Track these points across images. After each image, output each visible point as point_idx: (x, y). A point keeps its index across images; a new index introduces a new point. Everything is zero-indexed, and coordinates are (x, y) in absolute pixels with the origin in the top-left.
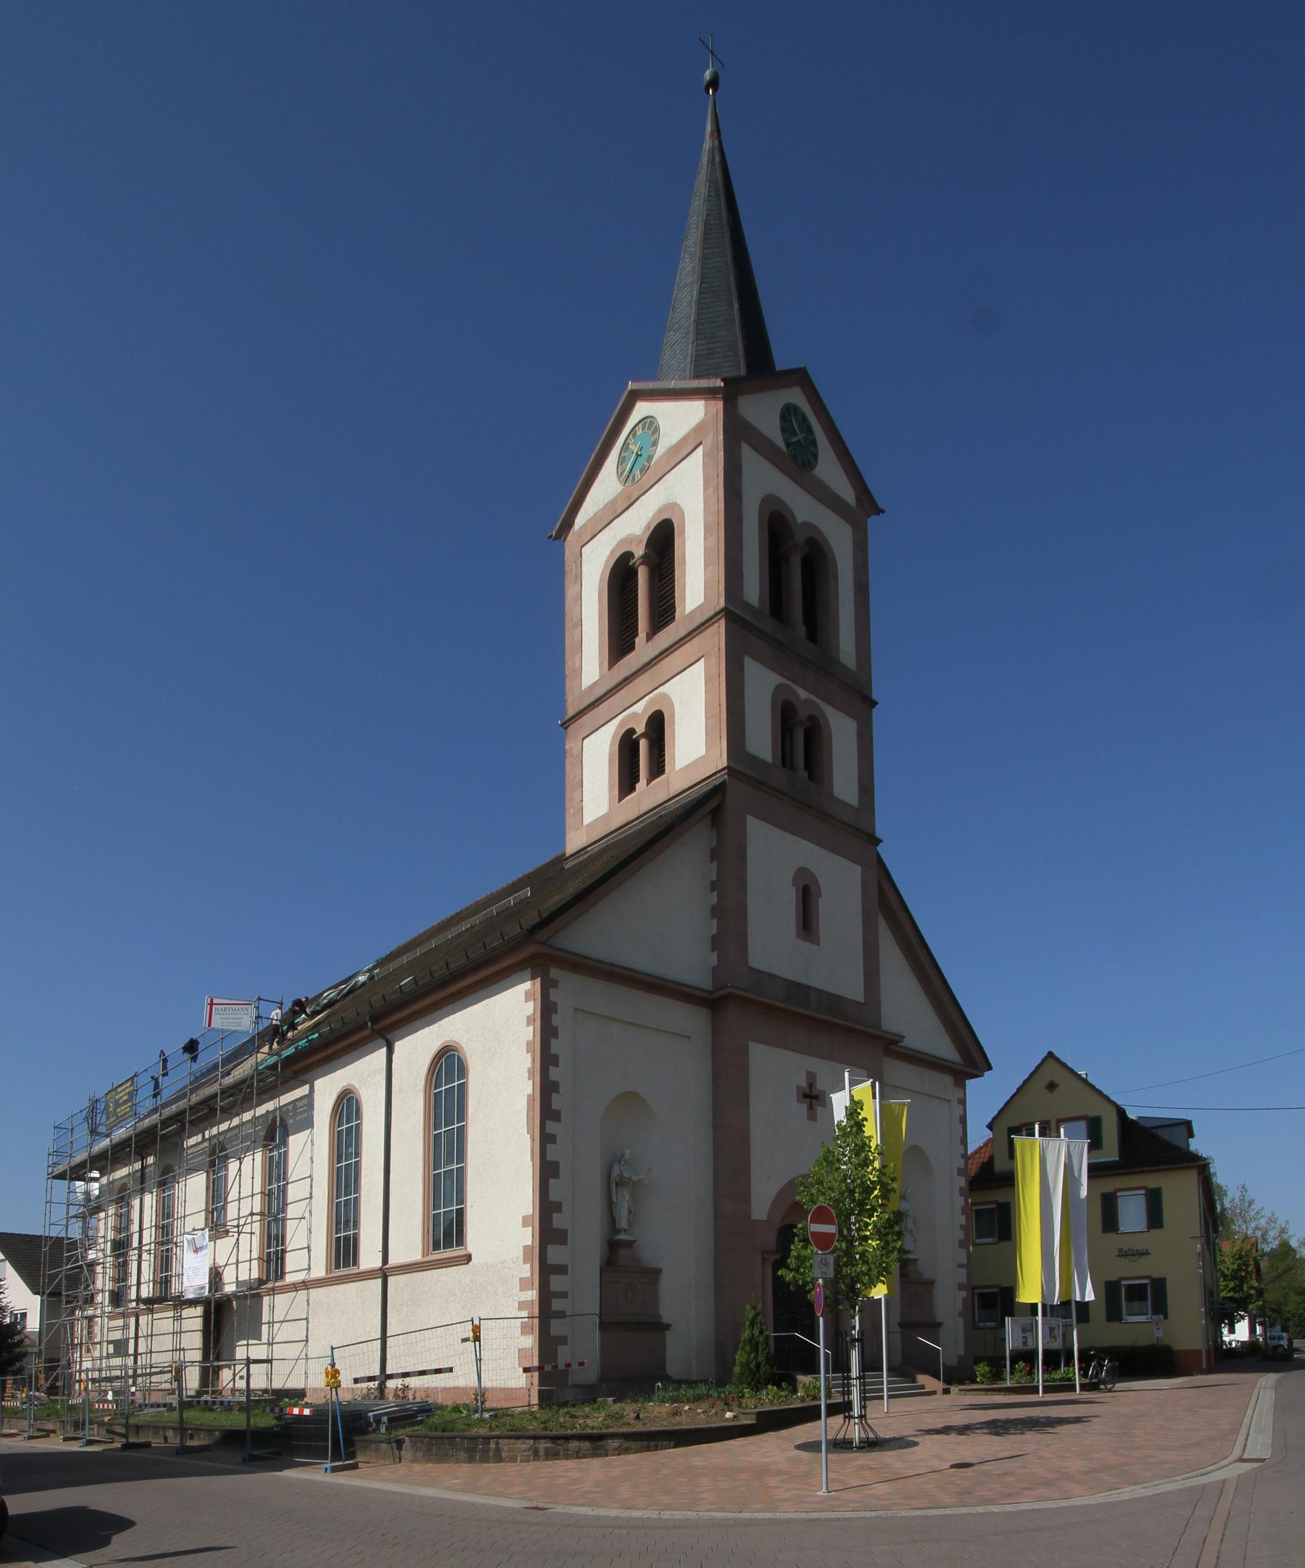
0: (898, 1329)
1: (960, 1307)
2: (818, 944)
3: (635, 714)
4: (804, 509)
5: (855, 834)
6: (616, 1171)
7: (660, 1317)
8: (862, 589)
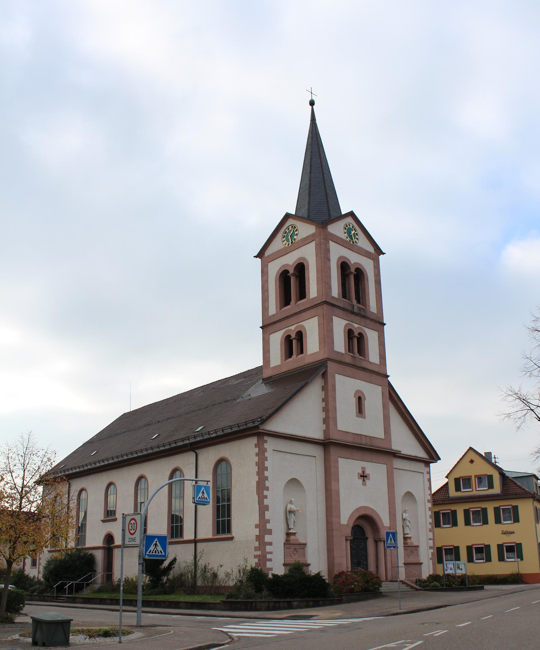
0: (404, 565)
1: (430, 556)
2: (365, 418)
3: (291, 330)
4: (354, 258)
5: (379, 375)
6: (288, 508)
7: (306, 561)
8: (378, 282)
